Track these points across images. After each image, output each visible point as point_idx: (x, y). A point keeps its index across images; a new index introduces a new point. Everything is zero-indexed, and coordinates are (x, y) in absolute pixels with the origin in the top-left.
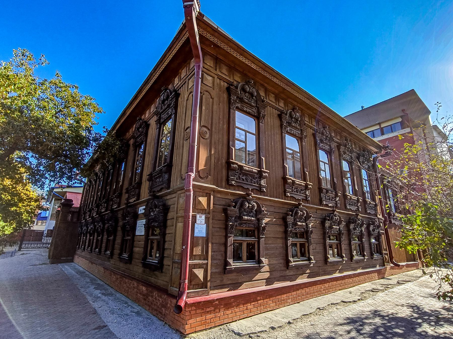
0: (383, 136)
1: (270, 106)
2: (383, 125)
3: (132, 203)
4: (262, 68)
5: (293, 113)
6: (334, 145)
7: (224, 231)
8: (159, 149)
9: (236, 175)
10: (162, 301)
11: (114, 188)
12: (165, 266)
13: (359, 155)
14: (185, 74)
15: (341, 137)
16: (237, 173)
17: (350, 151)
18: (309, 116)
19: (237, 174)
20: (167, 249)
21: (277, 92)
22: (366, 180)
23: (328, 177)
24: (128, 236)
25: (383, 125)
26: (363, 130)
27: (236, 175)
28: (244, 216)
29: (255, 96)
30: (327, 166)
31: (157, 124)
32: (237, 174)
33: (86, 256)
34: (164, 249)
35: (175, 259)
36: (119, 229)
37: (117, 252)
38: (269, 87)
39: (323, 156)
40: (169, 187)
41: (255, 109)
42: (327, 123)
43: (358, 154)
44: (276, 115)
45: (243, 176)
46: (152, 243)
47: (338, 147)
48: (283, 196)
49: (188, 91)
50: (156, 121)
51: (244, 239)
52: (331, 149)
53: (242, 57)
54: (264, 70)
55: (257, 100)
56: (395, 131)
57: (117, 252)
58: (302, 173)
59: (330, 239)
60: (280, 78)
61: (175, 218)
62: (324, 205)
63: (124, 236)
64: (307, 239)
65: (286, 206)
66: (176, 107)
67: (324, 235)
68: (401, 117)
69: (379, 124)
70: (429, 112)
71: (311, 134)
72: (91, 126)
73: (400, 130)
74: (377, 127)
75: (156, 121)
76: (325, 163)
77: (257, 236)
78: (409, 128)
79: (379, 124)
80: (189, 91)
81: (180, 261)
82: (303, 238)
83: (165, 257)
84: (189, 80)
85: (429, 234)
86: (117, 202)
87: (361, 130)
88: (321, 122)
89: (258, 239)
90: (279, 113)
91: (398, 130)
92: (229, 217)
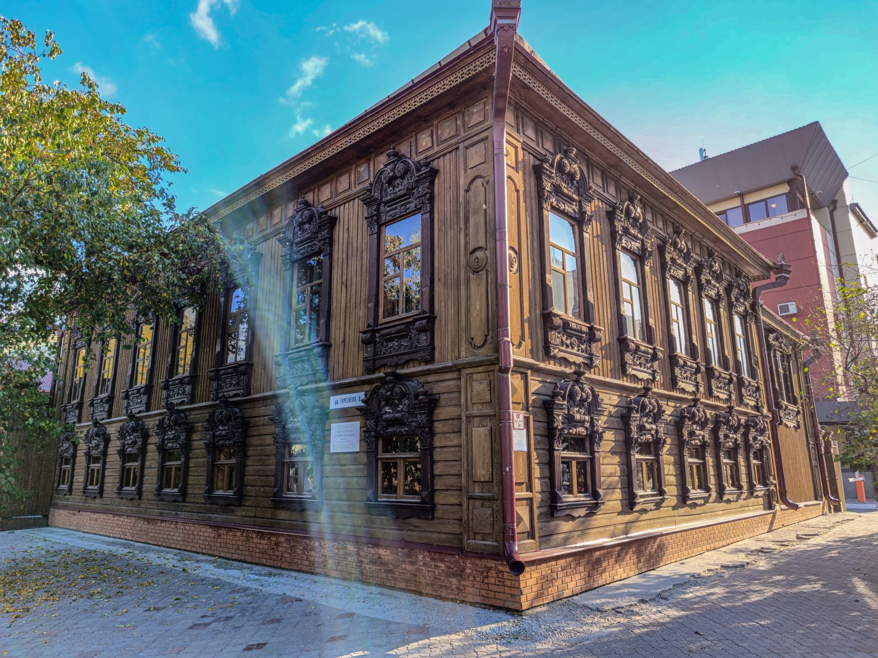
0: (749, 225)
1: (598, 198)
2: (748, 199)
4: (590, 124)
5: (631, 207)
6: (651, 243)
7: (546, 440)
10: (448, 567)
12: (438, 507)
13: (663, 242)
14: (453, 133)
15: (618, 190)
17: (684, 258)
18: (516, 109)
20: (440, 475)
21: (604, 164)
22: (630, 284)
23: (638, 316)
24: (66, 464)
25: (748, 199)
26: (712, 207)
29: (577, 181)
30: (635, 290)
31: (370, 225)
33: (88, 505)
35: (474, 492)
38: (595, 158)
39: (627, 269)
40: (431, 360)
41: (576, 205)
42: (685, 224)
43: (614, 207)
44: (603, 214)
45: (567, 339)
46: (65, 471)
47: (661, 250)
48: (621, 375)
49: (466, 171)
50: (366, 218)
51: (643, 457)
52: (643, 249)
53: (563, 105)
54: (595, 128)
55: (578, 187)
56: (775, 216)
58: (645, 328)
60: (578, 107)
61: (464, 418)
62: (629, 377)
64: (592, 452)
66: (431, 200)
67: (680, 444)
68: (789, 182)
69: (741, 196)
70: (846, 175)
71: (604, 213)
73: (785, 213)
74: (737, 203)
75: (366, 218)
76: (630, 284)
77: (589, 451)
78: (805, 211)
79: (741, 196)
80: (472, 174)
82: (649, 453)
83: (437, 490)
84: (467, 148)
85: (11, 344)
87: (708, 205)
88: (624, 188)
89: (655, 456)
90: (659, 242)
91: (781, 214)
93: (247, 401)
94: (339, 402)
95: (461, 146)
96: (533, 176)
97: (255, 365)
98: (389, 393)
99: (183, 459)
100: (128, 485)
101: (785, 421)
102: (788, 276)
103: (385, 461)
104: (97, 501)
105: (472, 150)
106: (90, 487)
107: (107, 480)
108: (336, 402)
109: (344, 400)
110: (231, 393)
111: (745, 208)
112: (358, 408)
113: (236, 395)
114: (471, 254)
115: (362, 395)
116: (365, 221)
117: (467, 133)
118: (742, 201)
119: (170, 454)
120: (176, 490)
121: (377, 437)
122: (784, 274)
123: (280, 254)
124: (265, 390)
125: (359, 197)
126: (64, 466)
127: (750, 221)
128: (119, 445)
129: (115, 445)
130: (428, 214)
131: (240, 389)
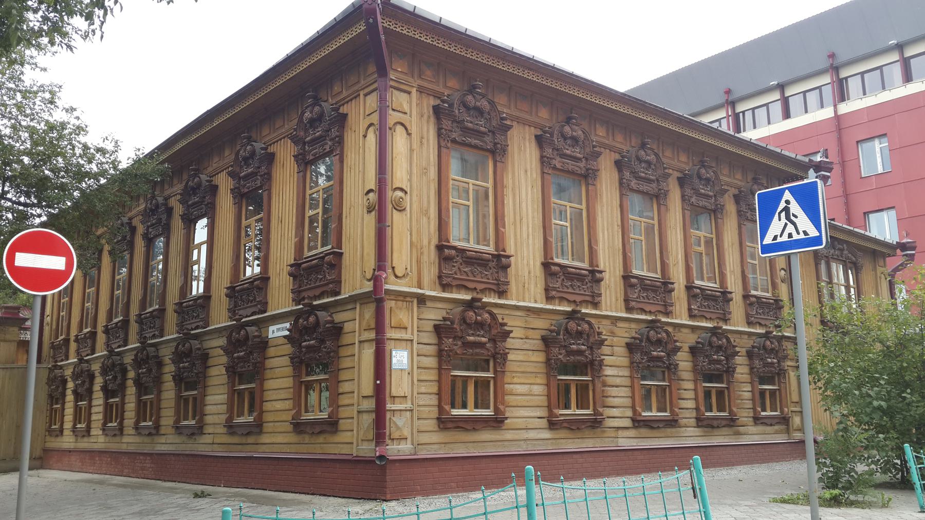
3: (247, 316)
8: (308, 192)
9: (454, 266)
11: (315, 303)
16: (456, 262)
19: (455, 264)
24: (57, 404)
25: (909, 53)
27: (454, 266)
28: (469, 335)
32: (455, 264)
34: (203, 415)
36: (130, 383)
37: (129, 422)
57: (129, 422)
59: (331, 425)
63: (139, 395)
65: (633, 326)
72: (841, 428)
74: (895, 56)
79: (781, 87)
81: (766, 287)
84: (366, 95)
86: (154, 326)
92: (444, 339)
93: (205, 333)
94: (275, 331)
95: (362, 93)
96: (432, 119)
97: (213, 298)
98: (305, 322)
99: (155, 393)
100: (111, 422)
101: (125, 362)
102: (828, 174)
103: (591, 388)
104: (86, 439)
105: (368, 97)
106: (79, 426)
107: (94, 417)
108: (273, 332)
109: (278, 330)
110: (194, 326)
111: (785, 102)
112: (285, 337)
113: (197, 328)
114: (366, 195)
115: (288, 325)
116: (293, 158)
117: (366, 81)
118: (783, 93)
119: (146, 388)
120: (150, 423)
121: (301, 362)
122: (823, 173)
123: (292, 154)
124: (221, 322)
125: (288, 136)
126: (55, 406)
127: (912, 80)
128: (102, 381)
129: (99, 381)
130: (337, 157)
131: (200, 321)
